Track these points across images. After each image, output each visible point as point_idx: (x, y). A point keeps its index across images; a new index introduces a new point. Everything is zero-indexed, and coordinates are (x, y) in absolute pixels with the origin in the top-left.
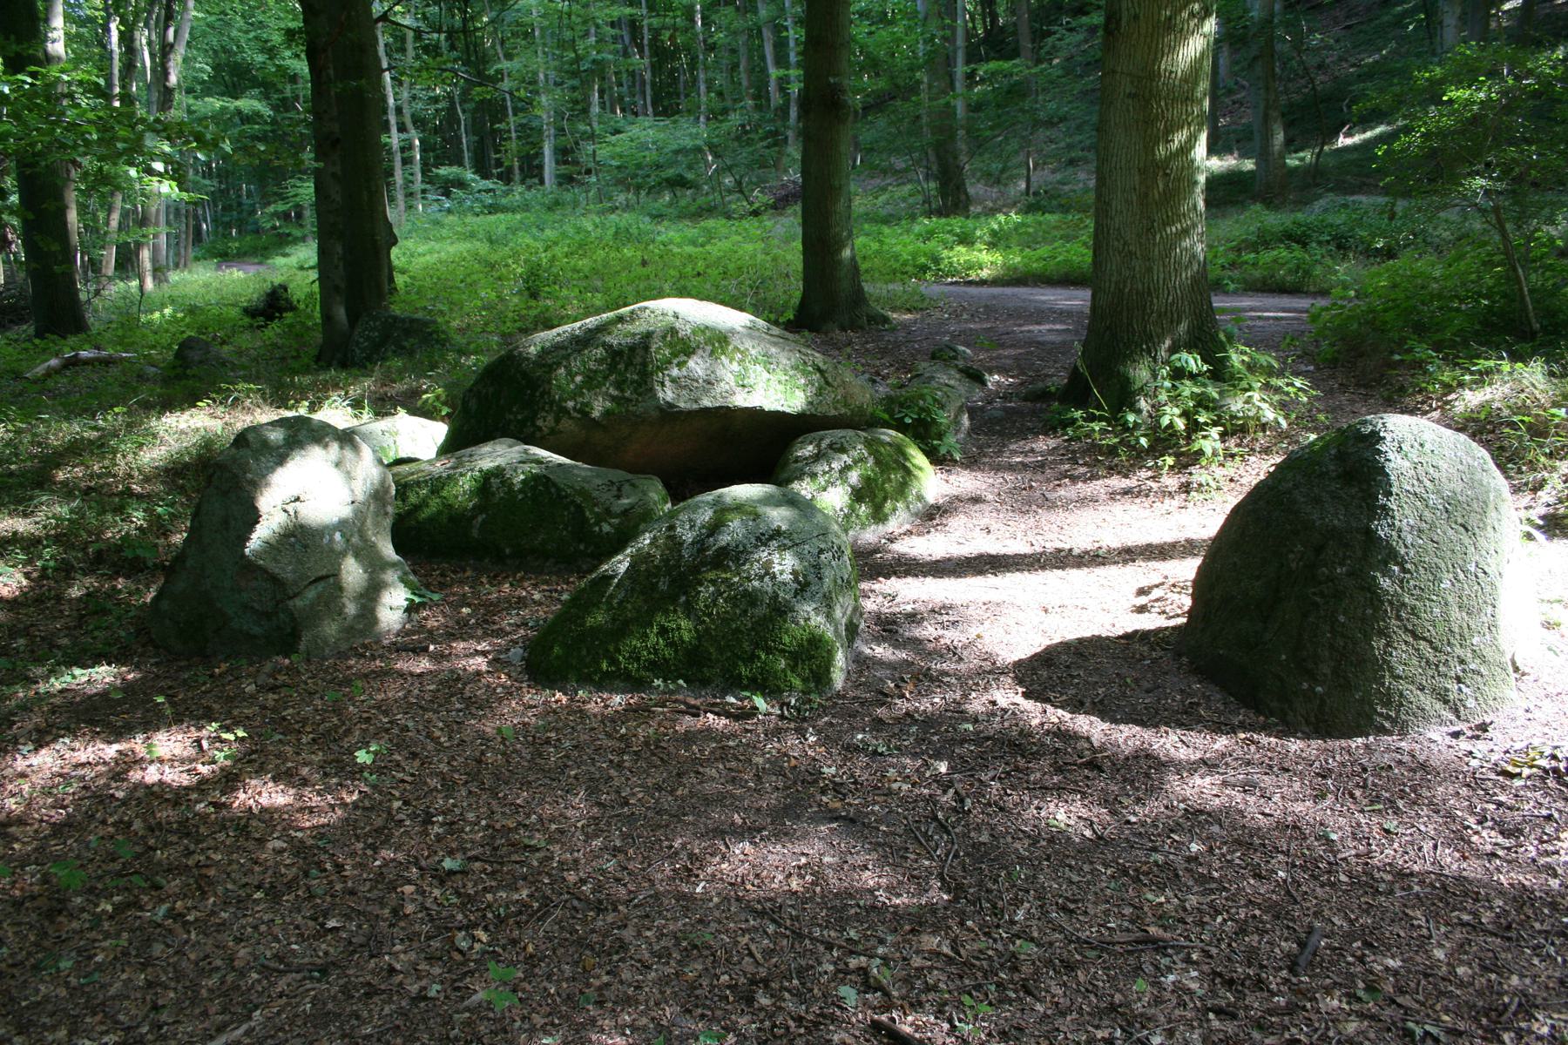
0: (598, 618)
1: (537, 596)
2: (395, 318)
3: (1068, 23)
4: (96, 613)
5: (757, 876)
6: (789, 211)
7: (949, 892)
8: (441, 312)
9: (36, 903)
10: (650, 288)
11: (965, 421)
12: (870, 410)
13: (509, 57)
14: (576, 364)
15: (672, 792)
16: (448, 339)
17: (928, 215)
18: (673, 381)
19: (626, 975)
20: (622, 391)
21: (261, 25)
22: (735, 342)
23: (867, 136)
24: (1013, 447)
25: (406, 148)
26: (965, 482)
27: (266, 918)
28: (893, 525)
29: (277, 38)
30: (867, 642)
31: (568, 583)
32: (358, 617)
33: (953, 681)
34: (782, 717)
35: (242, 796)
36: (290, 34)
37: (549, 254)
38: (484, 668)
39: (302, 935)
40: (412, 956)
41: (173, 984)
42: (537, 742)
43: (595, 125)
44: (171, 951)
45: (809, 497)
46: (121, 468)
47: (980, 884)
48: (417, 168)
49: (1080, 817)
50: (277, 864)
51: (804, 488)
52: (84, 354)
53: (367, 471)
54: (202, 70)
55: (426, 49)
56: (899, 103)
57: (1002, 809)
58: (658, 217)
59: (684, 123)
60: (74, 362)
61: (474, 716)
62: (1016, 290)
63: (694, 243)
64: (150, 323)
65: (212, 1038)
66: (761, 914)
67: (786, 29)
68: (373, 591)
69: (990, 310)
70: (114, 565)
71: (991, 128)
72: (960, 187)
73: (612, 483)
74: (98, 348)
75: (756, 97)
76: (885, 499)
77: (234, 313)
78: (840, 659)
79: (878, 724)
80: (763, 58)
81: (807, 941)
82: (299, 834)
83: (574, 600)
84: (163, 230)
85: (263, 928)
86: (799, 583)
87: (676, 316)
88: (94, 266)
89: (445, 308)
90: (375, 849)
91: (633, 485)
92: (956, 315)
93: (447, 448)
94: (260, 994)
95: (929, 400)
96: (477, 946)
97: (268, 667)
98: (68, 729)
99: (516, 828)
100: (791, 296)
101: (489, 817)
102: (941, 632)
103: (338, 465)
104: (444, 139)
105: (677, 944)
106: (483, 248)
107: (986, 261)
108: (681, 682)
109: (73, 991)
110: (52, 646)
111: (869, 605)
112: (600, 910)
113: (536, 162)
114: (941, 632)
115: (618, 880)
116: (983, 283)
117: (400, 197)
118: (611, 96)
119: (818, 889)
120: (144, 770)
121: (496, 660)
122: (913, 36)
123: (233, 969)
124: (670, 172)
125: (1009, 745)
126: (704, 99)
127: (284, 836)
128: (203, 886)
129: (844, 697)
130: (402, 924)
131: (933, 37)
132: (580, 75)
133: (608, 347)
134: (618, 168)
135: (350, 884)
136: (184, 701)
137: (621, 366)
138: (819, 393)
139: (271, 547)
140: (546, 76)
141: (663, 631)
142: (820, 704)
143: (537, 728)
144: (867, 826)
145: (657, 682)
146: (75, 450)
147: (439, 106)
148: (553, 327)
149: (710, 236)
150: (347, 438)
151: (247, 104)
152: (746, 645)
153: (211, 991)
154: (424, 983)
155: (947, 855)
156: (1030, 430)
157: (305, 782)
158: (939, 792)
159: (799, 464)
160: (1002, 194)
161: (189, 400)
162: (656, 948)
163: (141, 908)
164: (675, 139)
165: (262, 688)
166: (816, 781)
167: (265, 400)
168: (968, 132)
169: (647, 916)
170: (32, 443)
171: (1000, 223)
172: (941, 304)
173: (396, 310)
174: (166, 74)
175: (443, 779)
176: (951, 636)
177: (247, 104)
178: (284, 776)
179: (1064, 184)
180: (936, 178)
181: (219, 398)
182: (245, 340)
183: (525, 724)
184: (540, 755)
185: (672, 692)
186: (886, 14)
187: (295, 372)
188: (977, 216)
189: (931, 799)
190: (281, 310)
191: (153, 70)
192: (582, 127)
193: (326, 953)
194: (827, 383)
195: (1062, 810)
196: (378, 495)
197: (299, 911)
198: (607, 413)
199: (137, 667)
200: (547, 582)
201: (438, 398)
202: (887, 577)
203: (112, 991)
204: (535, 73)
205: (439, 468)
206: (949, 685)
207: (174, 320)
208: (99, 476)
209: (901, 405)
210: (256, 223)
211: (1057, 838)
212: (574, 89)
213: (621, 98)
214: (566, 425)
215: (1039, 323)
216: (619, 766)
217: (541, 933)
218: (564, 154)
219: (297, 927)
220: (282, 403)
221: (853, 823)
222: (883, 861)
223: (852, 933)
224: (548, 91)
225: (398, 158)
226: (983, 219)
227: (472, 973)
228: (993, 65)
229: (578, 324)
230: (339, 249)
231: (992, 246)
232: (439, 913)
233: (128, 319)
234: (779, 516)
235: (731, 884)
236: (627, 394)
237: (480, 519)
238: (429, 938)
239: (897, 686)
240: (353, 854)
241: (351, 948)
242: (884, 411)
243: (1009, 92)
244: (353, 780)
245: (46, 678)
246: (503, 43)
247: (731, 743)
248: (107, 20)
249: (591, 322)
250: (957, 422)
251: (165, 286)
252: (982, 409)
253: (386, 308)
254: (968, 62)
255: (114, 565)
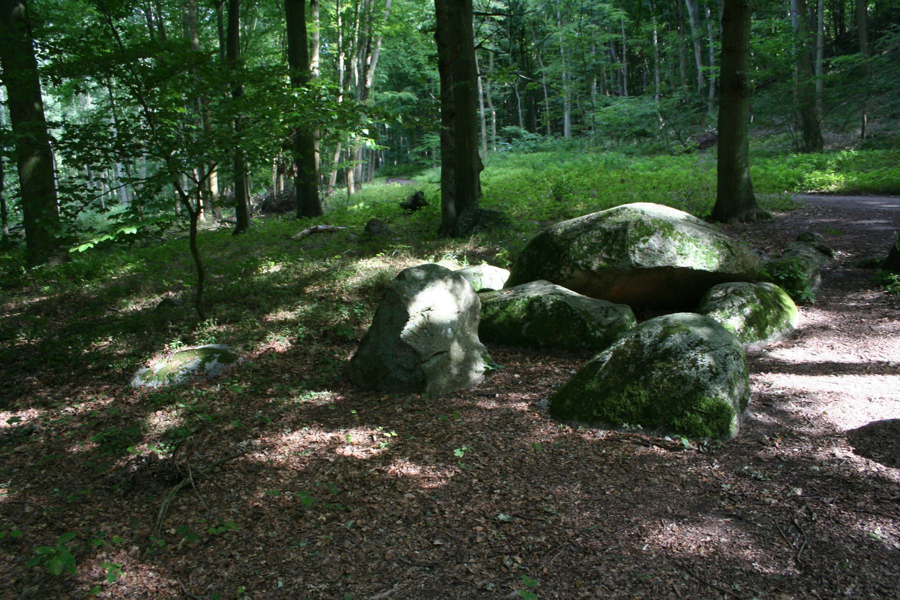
0: (593, 385)
1: (557, 371)
2: (482, 210)
3: (894, 27)
4: (323, 363)
5: (680, 544)
6: (708, 150)
7: (800, 569)
8: (507, 208)
9: (290, 511)
10: (625, 196)
11: (818, 279)
12: (758, 271)
13: (546, 64)
14: (584, 239)
15: (631, 490)
16: (510, 223)
17: (796, 151)
18: (641, 250)
19: (599, 593)
20: (610, 255)
21: (414, 53)
22: (678, 228)
23: (757, 104)
24: (850, 296)
25: (489, 116)
26: (817, 317)
27: (403, 534)
28: (770, 341)
29: (422, 60)
30: (752, 411)
31: (575, 364)
32: (459, 375)
33: (807, 439)
34: (698, 452)
35: (393, 468)
36: (431, 58)
37: (567, 175)
38: (526, 409)
39: (421, 546)
40: (479, 566)
41: (354, 563)
42: (555, 453)
43: (594, 101)
44: (354, 545)
45: (719, 321)
46: (337, 288)
47: (821, 567)
48: (494, 127)
49: (891, 534)
50: (410, 506)
51: (717, 316)
52: (320, 227)
53: (467, 295)
54: (383, 78)
55: (500, 61)
56: (778, 84)
57: (837, 522)
58: (630, 154)
59: (646, 99)
60: (315, 231)
61: (519, 436)
62: (853, 198)
63: (651, 169)
64: (352, 211)
65: (373, 594)
66: (681, 568)
67: (708, 42)
68: (467, 364)
69: (836, 211)
70: (333, 338)
71: (839, 97)
72: (818, 134)
73: (603, 308)
74: (327, 224)
75: (689, 83)
76: (766, 325)
77: (395, 206)
78: (735, 421)
79: (758, 461)
80: (694, 60)
81: (709, 588)
82: (422, 492)
83: (580, 374)
84: (360, 161)
85: (401, 540)
86: (713, 373)
87: (643, 213)
88: (326, 181)
89: (509, 206)
90: (462, 505)
91: (615, 310)
92: (813, 213)
93: (509, 285)
94: (398, 575)
95: (796, 265)
96: (516, 565)
97: (409, 399)
98: (307, 423)
99: (540, 501)
100: (710, 202)
101: (525, 493)
102: (800, 408)
103: (452, 291)
104: (509, 111)
105: (630, 579)
106: (530, 172)
107: (834, 180)
108: (639, 426)
109: (307, 559)
110: (301, 379)
111: (754, 388)
112: (586, 552)
113: (560, 123)
114: (800, 408)
115: (597, 538)
116: (831, 193)
117: (484, 143)
118: (604, 84)
119: (717, 557)
120: (344, 448)
121: (533, 405)
122: (789, 43)
123: (385, 560)
124: (638, 128)
125: (843, 483)
126: (658, 85)
127: (414, 491)
128: (371, 514)
129: (737, 443)
130: (475, 547)
131: (802, 42)
132: (586, 74)
133: (603, 230)
134: (607, 126)
135: (448, 522)
136: (365, 413)
137: (610, 241)
138: (727, 259)
139: (414, 334)
140: (567, 75)
141: (630, 396)
142: (722, 446)
143: (555, 446)
144: (749, 522)
145: (625, 425)
146: (316, 277)
147: (507, 93)
148: (572, 218)
149: (661, 165)
150: (457, 277)
151: (405, 94)
152: (679, 407)
153: (372, 569)
154: (485, 581)
155: (800, 546)
156: (862, 286)
157: (426, 463)
158: (796, 507)
159: (714, 302)
160: (845, 138)
161: (372, 253)
162: (618, 579)
163: (340, 521)
164: (642, 108)
165: (406, 411)
166: (718, 492)
167: (411, 254)
168: (823, 100)
169: (613, 560)
170: (295, 273)
171: (843, 156)
172: (804, 207)
173: (482, 206)
174: (365, 81)
175: (501, 469)
176: (806, 411)
177: (405, 94)
178: (416, 459)
179: (888, 130)
180: (801, 129)
181: (388, 252)
182: (401, 221)
183: (548, 443)
184: (556, 461)
185: (633, 431)
186: (771, 30)
187: (426, 239)
188: (828, 152)
189: (790, 510)
190: (420, 205)
191: (359, 79)
192: (587, 103)
193: (433, 558)
194: (732, 254)
195: (879, 528)
196: (472, 309)
197: (420, 533)
198: (601, 268)
199: (342, 394)
200: (563, 363)
201: (504, 255)
202: (767, 372)
203: (325, 562)
204: (561, 73)
205: (506, 295)
206: (804, 441)
207: (364, 210)
208: (327, 292)
209: (778, 269)
210: (407, 158)
211: (874, 544)
212: (582, 81)
213: (609, 85)
214: (577, 273)
215: (868, 219)
216: (601, 471)
217: (552, 563)
218: (576, 119)
219: (419, 542)
220: (420, 256)
221: (740, 519)
222: (757, 545)
223: (737, 587)
224: (567, 84)
225: (484, 122)
226: (832, 154)
227: (512, 579)
228: (841, 58)
229: (586, 216)
230: (453, 173)
231: (838, 170)
232: (495, 544)
233: (341, 209)
234: (702, 332)
235: (664, 548)
236: (613, 257)
237: (527, 325)
238: (489, 557)
239: (771, 439)
240: (450, 506)
241: (446, 557)
242: (768, 272)
243: (851, 74)
244: (452, 465)
245: (298, 395)
246: (542, 57)
247: (667, 465)
248: (338, 55)
249: (593, 215)
250: (813, 279)
251: (360, 191)
252: (829, 272)
253: (477, 205)
254: (824, 56)
255: (333, 338)
